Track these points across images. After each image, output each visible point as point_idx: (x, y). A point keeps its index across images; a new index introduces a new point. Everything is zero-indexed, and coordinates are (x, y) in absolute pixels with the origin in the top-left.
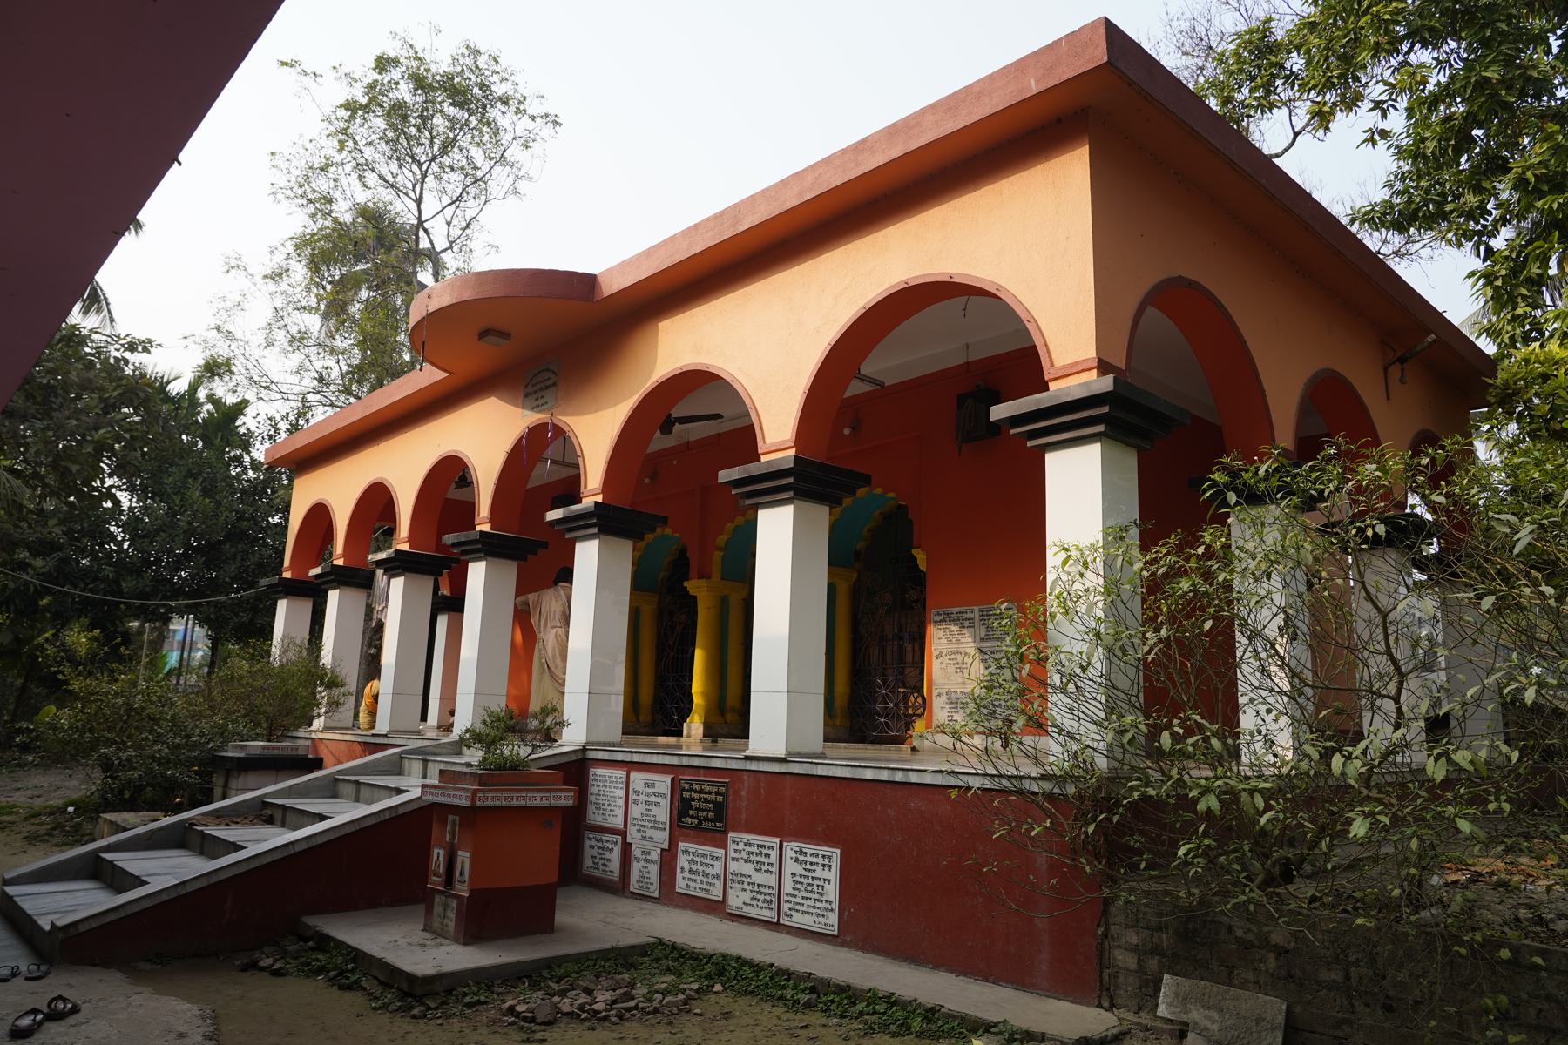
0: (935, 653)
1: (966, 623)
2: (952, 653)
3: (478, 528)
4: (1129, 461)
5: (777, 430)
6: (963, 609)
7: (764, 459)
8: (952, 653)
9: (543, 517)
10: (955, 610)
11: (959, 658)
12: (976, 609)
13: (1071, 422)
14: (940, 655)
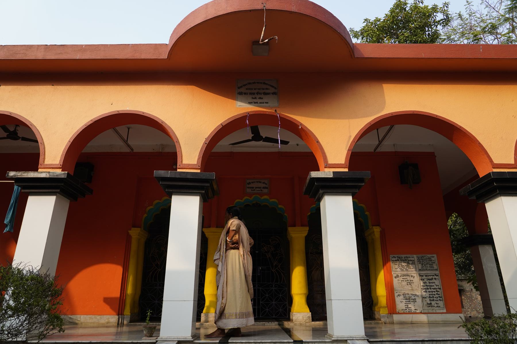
0: (394, 275)
1: (411, 262)
2: (404, 275)
3: (178, 170)
4: (66, 204)
5: (190, 158)
6: (408, 256)
7: (178, 170)
8: (404, 275)
9: (308, 173)
10: (403, 256)
12: (415, 256)
13: (186, 185)
14: (397, 276)
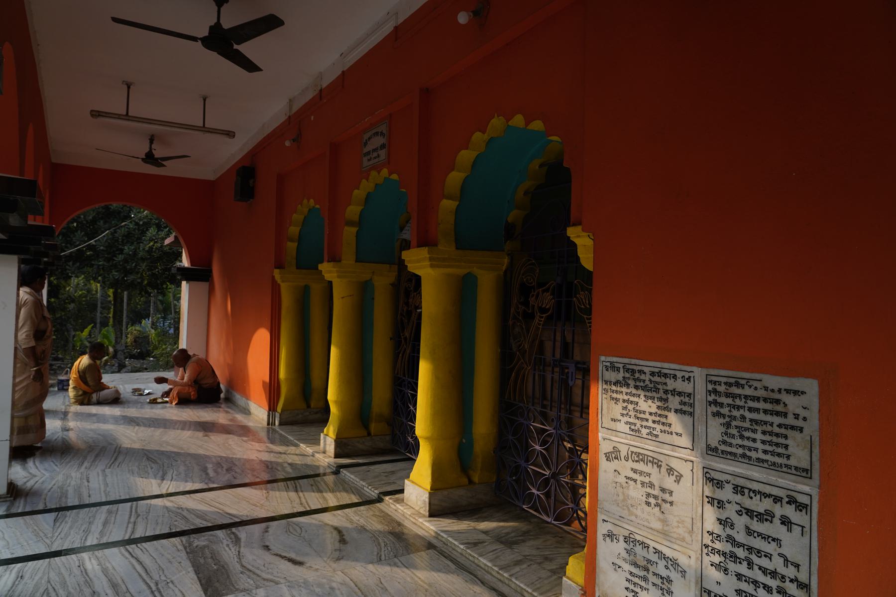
0: (605, 447)
1: (674, 402)
2: (640, 458)
6: (668, 367)
8: (640, 458)
11: (656, 476)
12: (698, 373)
